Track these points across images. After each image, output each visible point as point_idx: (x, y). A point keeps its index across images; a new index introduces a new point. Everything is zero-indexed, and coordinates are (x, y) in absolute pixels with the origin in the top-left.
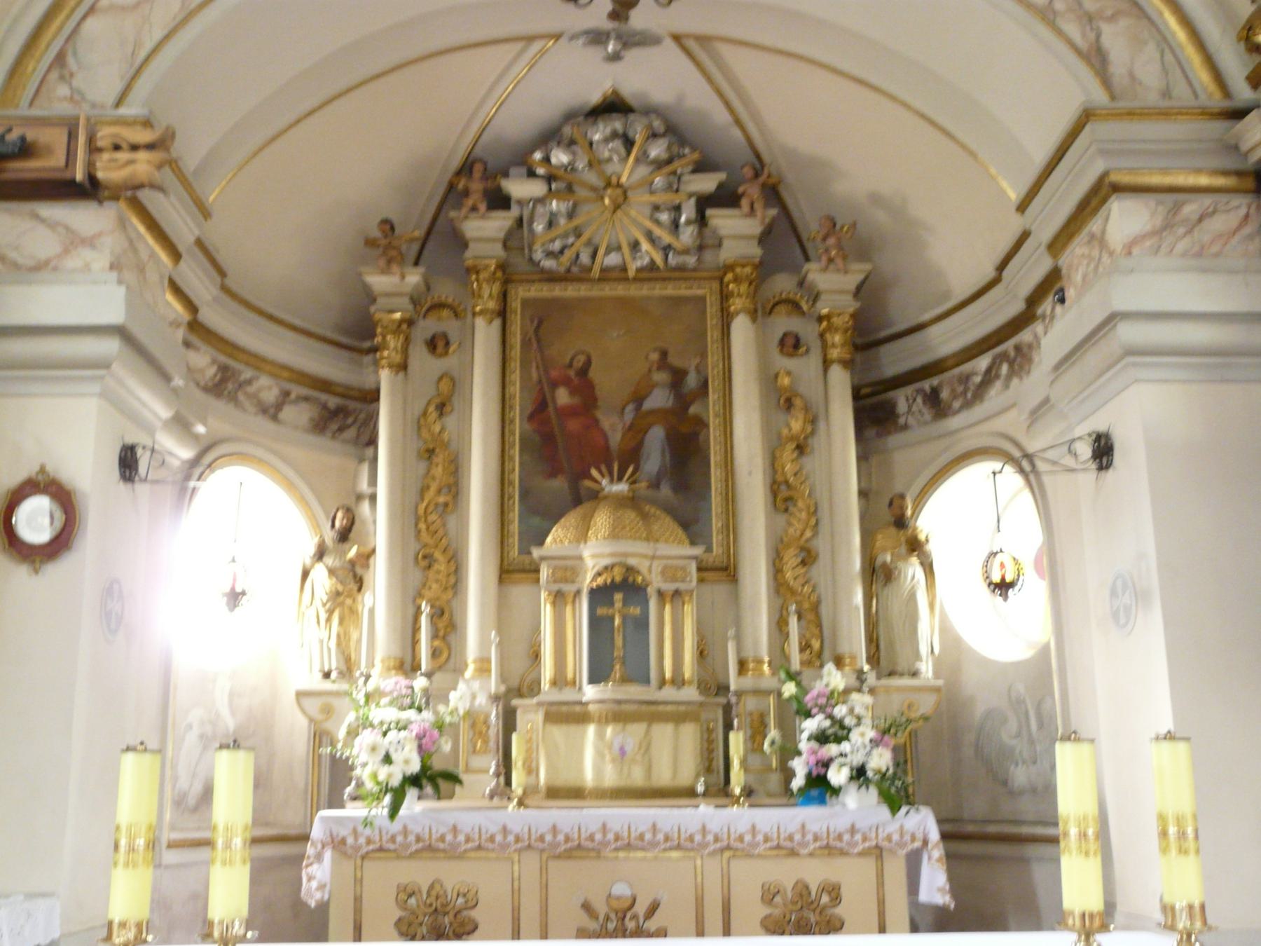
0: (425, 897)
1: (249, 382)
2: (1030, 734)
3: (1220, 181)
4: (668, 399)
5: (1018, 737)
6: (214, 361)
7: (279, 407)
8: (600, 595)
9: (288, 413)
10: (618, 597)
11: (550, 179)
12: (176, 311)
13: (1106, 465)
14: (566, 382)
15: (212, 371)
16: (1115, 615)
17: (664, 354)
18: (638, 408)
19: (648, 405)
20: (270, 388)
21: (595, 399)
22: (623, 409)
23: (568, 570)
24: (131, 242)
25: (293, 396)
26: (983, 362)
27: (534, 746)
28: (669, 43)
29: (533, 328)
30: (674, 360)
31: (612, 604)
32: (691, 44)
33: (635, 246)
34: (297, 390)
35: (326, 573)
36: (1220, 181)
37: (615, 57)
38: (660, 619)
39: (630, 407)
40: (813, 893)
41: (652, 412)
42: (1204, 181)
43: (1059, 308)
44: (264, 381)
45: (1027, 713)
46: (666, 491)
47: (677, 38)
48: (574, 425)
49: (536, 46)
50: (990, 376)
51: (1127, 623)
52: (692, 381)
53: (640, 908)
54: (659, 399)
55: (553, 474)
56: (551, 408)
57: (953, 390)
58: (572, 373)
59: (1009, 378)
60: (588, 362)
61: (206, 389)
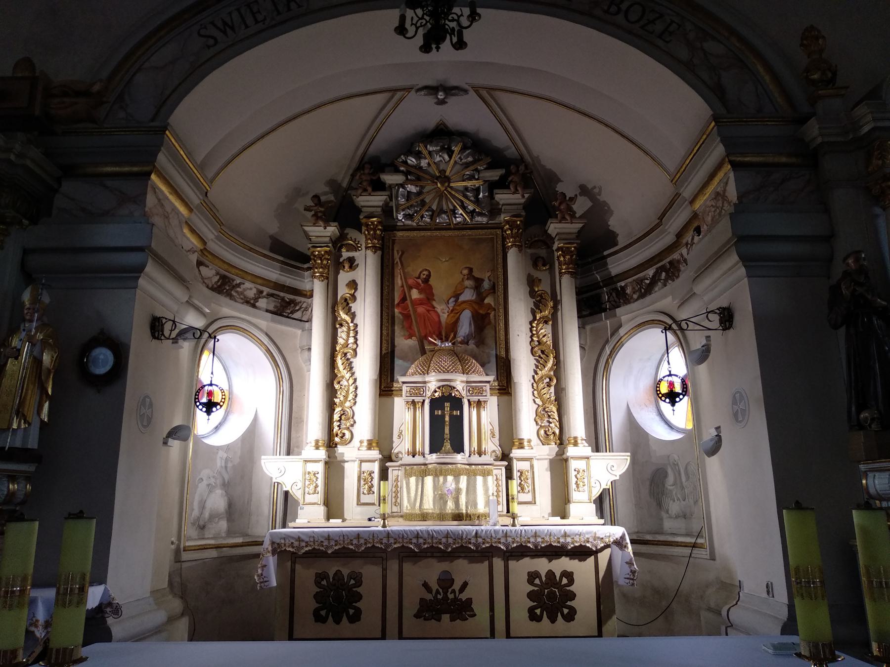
0: (331, 580)
1: (239, 285)
2: (681, 483)
3: (793, 160)
4: (473, 295)
5: (674, 485)
6: (217, 274)
7: (256, 299)
8: (436, 404)
9: (262, 303)
10: (447, 404)
11: (406, 174)
12: (193, 243)
13: (729, 327)
14: (417, 286)
15: (217, 278)
16: (735, 415)
17: (471, 270)
18: (456, 301)
19: (462, 298)
20: (251, 289)
21: (433, 295)
22: (448, 301)
23: (418, 389)
24: (159, 200)
25: (265, 293)
26: (651, 272)
27: (399, 489)
28: (472, 93)
29: (399, 256)
30: (476, 274)
31: (443, 409)
32: (484, 93)
33: (454, 212)
34: (266, 290)
35: (404, 403)
36: (793, 160)
37: (442, 102)
38: (469, 415)
39: (452, 299)
40: (558, 578)
41: (464, 302)
42: (784, 160)
43: (696, 239)
44: (248, 285)
45: (679, 471)
46: (472, 346)
47: (477, 90)
48: (421, 309)
49: (399, 95)
50: (654, 280)
51: (744, 419)
52: (486, 285)
53: (457, 586)
54: (468, 295)
55: (410, 337)
56: (408, 301)
57: (633, 288)
58: (420, 281)
59: (666, 280)
60: (429, 276)
61: (212, 289)
